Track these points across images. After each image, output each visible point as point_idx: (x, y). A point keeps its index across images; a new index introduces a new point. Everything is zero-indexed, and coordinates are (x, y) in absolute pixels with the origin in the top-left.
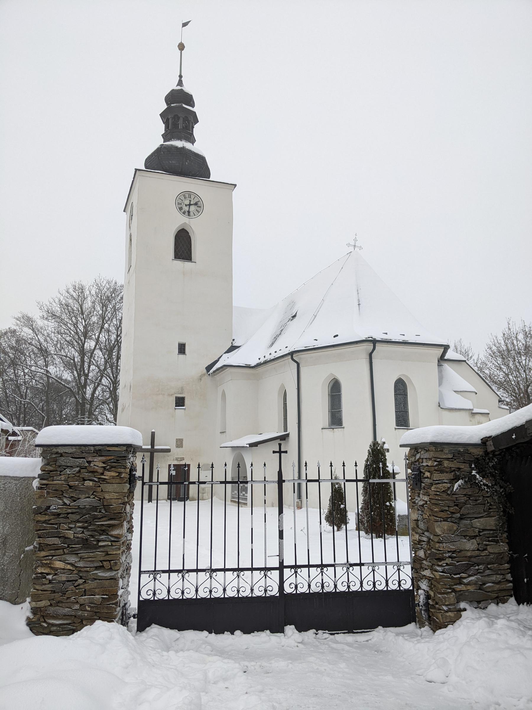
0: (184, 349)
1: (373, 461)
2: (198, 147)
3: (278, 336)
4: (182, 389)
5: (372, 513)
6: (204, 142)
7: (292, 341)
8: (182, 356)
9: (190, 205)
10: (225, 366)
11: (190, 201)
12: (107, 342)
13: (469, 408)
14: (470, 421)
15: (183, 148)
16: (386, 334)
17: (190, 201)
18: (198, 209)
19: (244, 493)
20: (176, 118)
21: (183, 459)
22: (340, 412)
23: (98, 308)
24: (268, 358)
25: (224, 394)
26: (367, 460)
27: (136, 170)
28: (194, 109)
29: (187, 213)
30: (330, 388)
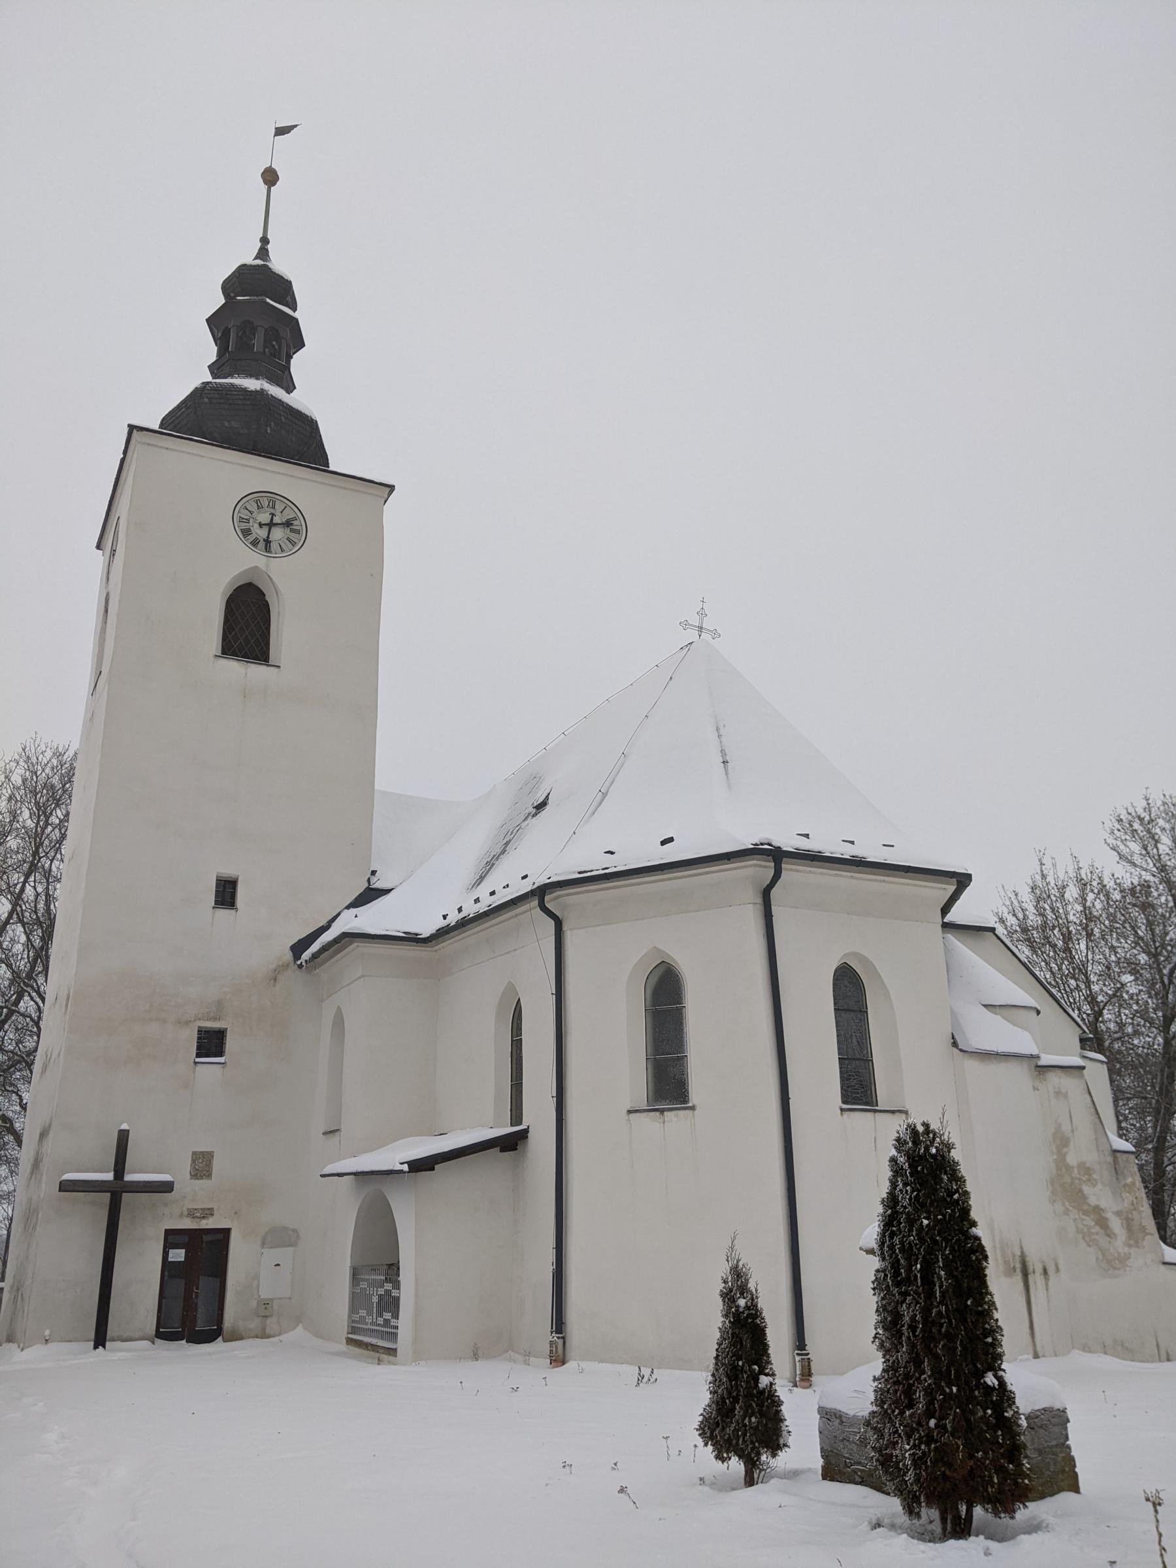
0: (233, 895)
1: (916, 1202)
2: (303, 397)
3: (497, 857)
4: (220, 1004)
5: (932, 1423)
6: (314, 385)
7: (542, 857)
8: (224, 914)
10: (345, 935)
11: (273, 515)
12: (41, 905)
13: (1028, 1052)
14: (1035, 1089)
15: (262, 392)
16: (807, 836)
17: (273, 515)
18: (293, 536)
19: (387, 1316)
20: (247, 329)
21: (208, 1213)
22: (681, 1061)
23: (26, 818)
24: (470, 909)
25: (339, 1022)
26: (891, 1201)
27: (132, 428)
28: (296, 315)
29: (262, 544)
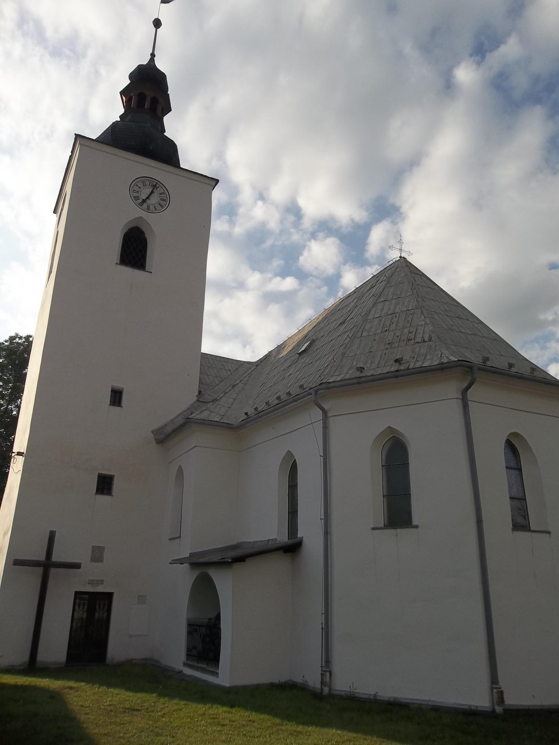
9: (151, 194)
25: (180, 471)
30: (384, 457)
